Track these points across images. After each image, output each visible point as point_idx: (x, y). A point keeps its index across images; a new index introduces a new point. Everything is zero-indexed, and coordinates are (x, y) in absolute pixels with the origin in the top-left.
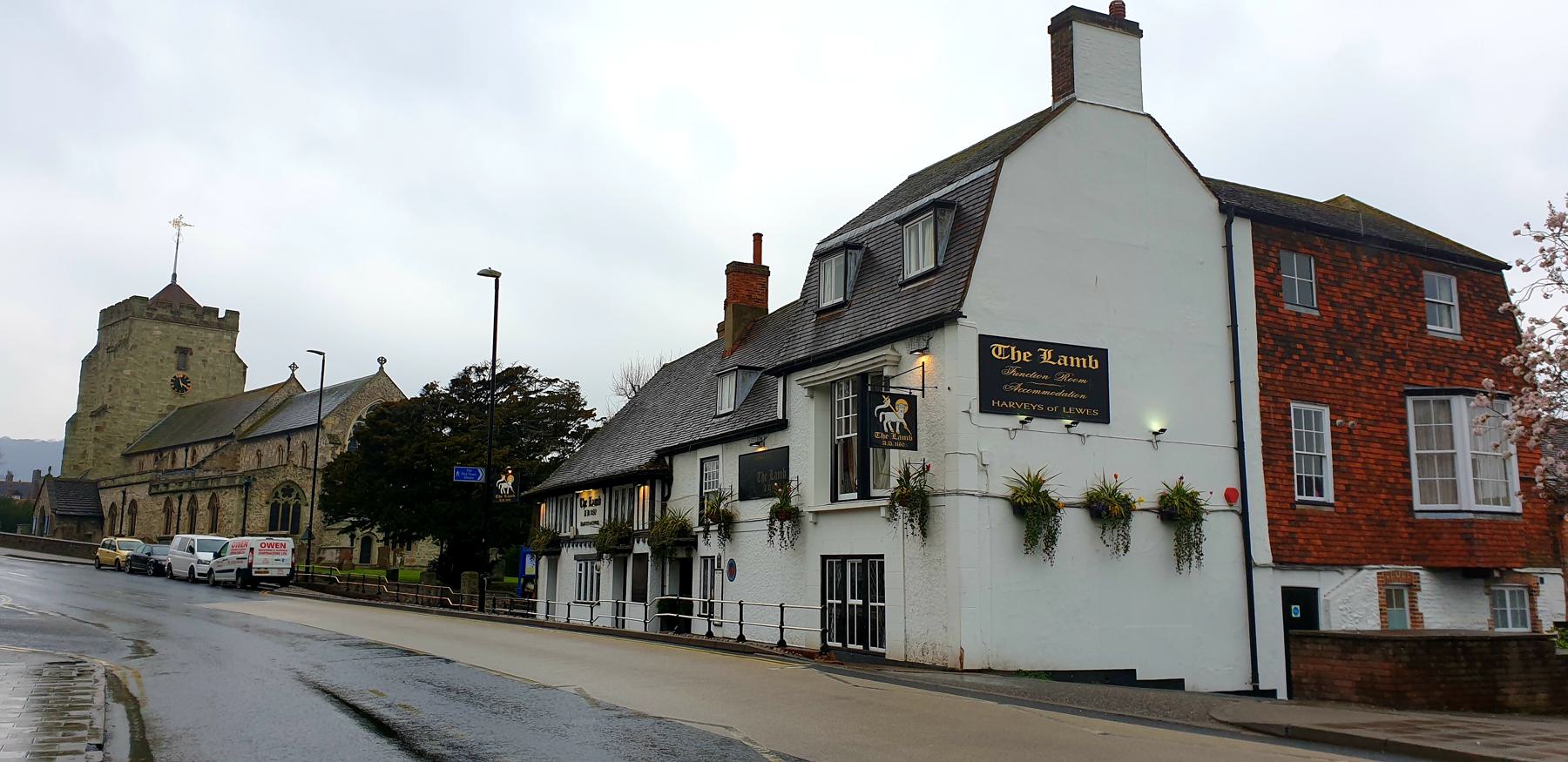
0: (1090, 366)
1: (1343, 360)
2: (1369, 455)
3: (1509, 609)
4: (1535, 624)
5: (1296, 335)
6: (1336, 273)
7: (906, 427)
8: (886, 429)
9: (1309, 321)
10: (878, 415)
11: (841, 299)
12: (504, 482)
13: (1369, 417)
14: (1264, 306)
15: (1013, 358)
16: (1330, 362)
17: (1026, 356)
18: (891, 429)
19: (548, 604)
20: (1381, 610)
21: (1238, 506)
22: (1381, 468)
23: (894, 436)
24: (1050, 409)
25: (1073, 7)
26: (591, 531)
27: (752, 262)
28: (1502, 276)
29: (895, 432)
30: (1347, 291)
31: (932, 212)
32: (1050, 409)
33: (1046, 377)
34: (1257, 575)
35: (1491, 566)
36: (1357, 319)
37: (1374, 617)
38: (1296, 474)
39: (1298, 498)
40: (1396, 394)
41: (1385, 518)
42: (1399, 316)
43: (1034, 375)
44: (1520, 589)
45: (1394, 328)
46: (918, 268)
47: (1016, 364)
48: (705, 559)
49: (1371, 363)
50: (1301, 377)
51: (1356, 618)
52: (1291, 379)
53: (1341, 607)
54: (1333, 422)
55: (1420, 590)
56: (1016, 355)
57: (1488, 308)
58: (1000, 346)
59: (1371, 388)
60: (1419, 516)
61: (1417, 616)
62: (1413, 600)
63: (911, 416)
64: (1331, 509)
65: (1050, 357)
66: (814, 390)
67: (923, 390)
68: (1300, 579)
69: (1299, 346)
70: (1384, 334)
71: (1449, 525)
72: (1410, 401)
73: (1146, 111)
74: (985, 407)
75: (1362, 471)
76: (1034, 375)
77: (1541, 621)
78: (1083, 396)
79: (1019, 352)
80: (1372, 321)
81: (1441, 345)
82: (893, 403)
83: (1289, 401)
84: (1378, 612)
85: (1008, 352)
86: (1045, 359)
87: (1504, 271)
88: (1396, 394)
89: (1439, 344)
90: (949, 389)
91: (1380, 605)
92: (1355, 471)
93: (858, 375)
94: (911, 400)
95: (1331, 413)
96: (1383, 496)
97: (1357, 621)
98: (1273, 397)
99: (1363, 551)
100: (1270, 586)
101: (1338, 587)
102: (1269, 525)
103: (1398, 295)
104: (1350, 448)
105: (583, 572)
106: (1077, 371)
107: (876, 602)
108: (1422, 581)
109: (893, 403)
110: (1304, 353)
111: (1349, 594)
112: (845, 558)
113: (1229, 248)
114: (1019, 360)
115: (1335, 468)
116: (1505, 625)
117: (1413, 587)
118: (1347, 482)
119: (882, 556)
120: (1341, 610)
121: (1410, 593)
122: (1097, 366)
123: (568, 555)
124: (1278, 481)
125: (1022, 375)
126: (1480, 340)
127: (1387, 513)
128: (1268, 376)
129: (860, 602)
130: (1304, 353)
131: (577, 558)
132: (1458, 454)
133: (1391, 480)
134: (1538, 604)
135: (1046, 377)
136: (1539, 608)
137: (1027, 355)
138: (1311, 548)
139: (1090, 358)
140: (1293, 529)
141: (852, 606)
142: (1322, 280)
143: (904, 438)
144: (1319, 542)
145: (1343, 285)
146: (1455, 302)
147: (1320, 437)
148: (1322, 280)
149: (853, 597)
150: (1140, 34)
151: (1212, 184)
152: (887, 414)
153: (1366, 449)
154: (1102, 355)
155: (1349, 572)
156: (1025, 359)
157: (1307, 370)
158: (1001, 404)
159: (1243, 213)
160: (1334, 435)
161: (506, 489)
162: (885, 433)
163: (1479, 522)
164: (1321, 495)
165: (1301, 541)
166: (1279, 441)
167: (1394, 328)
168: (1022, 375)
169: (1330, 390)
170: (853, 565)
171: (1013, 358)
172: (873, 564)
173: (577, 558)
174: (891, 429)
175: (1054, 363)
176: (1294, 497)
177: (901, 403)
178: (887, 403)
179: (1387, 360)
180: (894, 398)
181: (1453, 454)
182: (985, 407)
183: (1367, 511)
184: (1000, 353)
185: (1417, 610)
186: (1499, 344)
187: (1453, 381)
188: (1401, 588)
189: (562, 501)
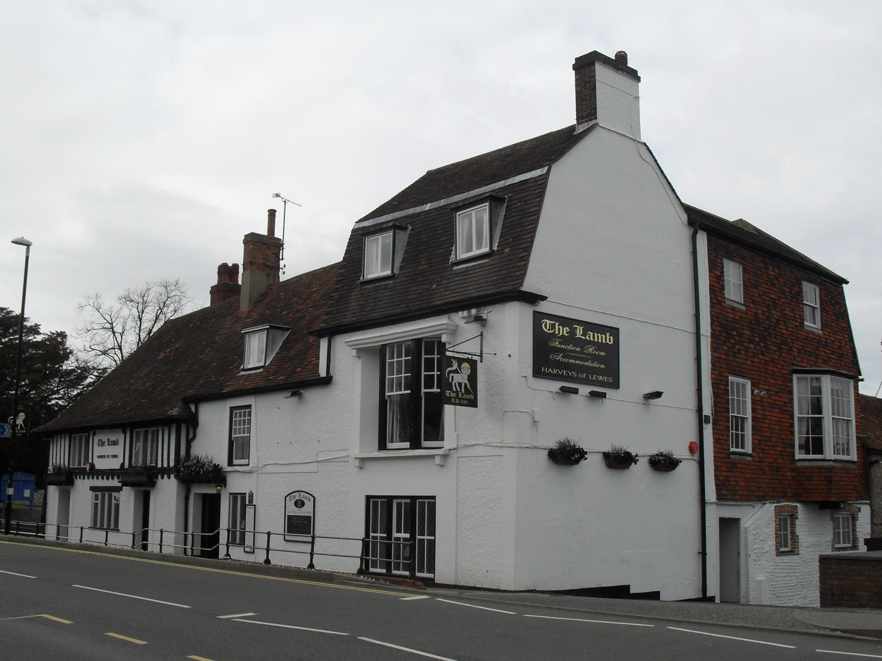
0: (608, 342)
1: (759, 345)
2: (773, 418)
3: (841, 531)
4: (855, 541)
5: (732, 324)
6: (755, 279)
7: (23, 426)
8: (454, 389)
9: (739, 314)
10: (449, 376)
11: (388, 272)
12: (456, 372)
13: (773, 389)
14: (715, 301)
15: (557, 332)
16: (752, 346)
17: (565, 331)
18: (458, 389)
19: (59, 527)
20: (776, 534)
21: (696, 456)
22: (778, 427)
23: (460, 395)
24: (581, 376)
25: (595, 51)
26: (115, 464)
27: (266, 234)
28: (842, 288)
29: (461, 391)
30: (761, 293)
31: (487, 204)
32: (581, 376)
33: (578, 349)
34: (708, 509)
35: (840, 500)
36: (767, 314)
37: (772, 539)
38: (731, 431)
39: (732, 450)
40: (787, 372)
41: (780, 466)
42: (790, 314)
43: (570, 347)
44: (847, 516)
45: (787, 322)
46: (469, 249)
47: (559, 338)
48: (234, 496)
49: (774, 348)
50: (735, 357)
51: (762, 540)
52: (730, 358)
53: (754, 533)
54: (752, 391)
55: (797, 518)
56: (559, 329)
57: (835, 311)
58: (548, 322)
59: (774, 367)
60: (799, 464)
61: (795, 537)
62: (793, 525)
63: (473, 378)
64: (750, 459)
65: (581, 333)
66: (362, 351)
67: (481, 356)
68: (729, 512)
69: (735, 333)
70: (781, 327)
71: (817, 470)
72: (795, 377)
73: (643, 140)
74: (538, 373)
75: (767, 430)
76: (570, 347)
77: (858, 538)
78: (603, 366)
79: (561, 327)
80: (775, 316)
81: (811, 337)
82: (459, 366)
83: (727, 374)
84: (774, 536)
85: (553, 326)
86: (578, 334)
87: (844, 285)
88: (787, 372)
89: (810, 335)
90: (510, 356)
91: (776, 531)
92: (763, 429)
93: (412, 340)
94: (473, 364)
95: (752, 385)
96: (779, 449)
97: (762, 542)
98: (719, 371)
99: (766, 490)
100: (713, 516)
101: (751, 517)
102: (715, 470)
103: (789, 298)
104: (762, 412)
105: (99, 502)
106: (601, 346)
107: (427, 540)
108: (799, 512)
109: (459, 366)
110: (737, 338)
111: (759, 522)
112: (390, 499)
113: (694, 253)
114: (561, 334)
115: (754, 427)
116: (839, 543)
117: (793, 517)
118: (759, 438)
119: (434, 497)
120: (754, 535)
121: (791, 521)
122: (612, 342)
123: (82, 489)
124: (721, 438)
125: (563, 346)
126: (831, 335)
127: (781, 461)
128: (716, 355)
129: (407, 536)
130: (737, 338)
131: (93, 489)
132: (825, 418)
133: (784, 437)
134: (857, 526)
135: (578, 349)
136: (858, 530)
137: (567, 330)
138: (738, 488)
139: (608, 334)
140: (729, 474)
141: (398, 539)
142: (748, 284)
143: (22, 431)
144: (742, 484)
145: (759, 288)
146: (818, 306)
147: (745, 402)
148: (748, 284)
149: (399, 531)
150: (638, 79)
151: (684, 205)
152: (455, 375)
153: (770, 414)
154: (615, 332)
155: (758, 505)
156: (565, 334)
157: (739, 351)
158: (548, 370)
159: (704, 228)
160: (754, 402)
161: (460, 384)
162: (454, 392)
163: (835, 468)
164: (743, 447)
165: (733, 483)
166: (721, 405)
167: (787, 322)
168: (563, 346)
169: (751, 368)
170: (399, 505)
171: (557, 332)
172: (422, 505)
173: (93, 489)
174: (458, 389)
175: (584, 338)
176: (730, 449)
177: (465, 365)
178: (455, 366)
179: (783, 347)
180: (460, 361)
181: (821, 418)
182: (538, 373)
183: (770, 460)
184: (548, 328)
185: (796, 533)
186: (840, 338)
187: (817, 364)
188: (786, 517)
189: (75, 438)
